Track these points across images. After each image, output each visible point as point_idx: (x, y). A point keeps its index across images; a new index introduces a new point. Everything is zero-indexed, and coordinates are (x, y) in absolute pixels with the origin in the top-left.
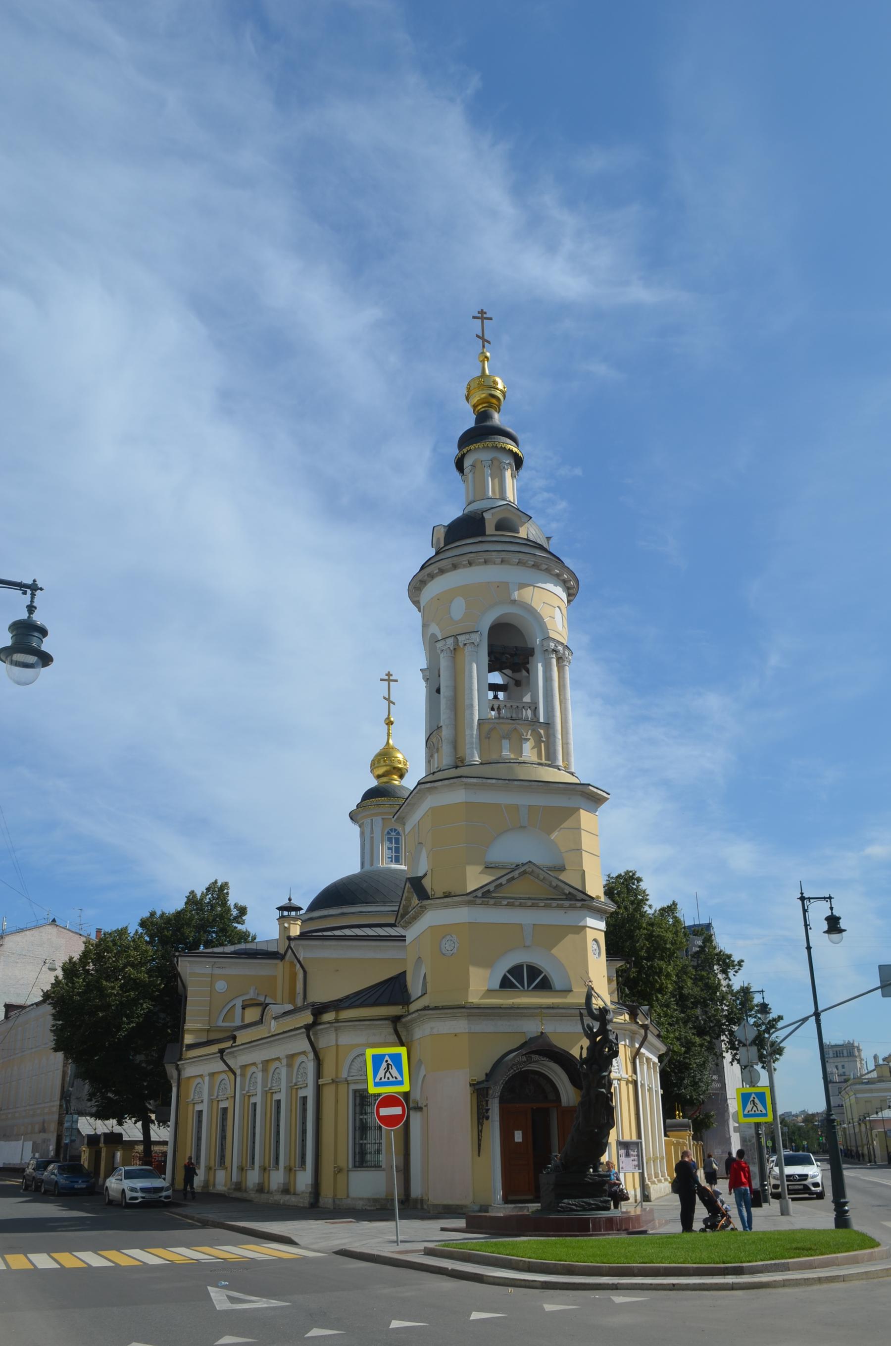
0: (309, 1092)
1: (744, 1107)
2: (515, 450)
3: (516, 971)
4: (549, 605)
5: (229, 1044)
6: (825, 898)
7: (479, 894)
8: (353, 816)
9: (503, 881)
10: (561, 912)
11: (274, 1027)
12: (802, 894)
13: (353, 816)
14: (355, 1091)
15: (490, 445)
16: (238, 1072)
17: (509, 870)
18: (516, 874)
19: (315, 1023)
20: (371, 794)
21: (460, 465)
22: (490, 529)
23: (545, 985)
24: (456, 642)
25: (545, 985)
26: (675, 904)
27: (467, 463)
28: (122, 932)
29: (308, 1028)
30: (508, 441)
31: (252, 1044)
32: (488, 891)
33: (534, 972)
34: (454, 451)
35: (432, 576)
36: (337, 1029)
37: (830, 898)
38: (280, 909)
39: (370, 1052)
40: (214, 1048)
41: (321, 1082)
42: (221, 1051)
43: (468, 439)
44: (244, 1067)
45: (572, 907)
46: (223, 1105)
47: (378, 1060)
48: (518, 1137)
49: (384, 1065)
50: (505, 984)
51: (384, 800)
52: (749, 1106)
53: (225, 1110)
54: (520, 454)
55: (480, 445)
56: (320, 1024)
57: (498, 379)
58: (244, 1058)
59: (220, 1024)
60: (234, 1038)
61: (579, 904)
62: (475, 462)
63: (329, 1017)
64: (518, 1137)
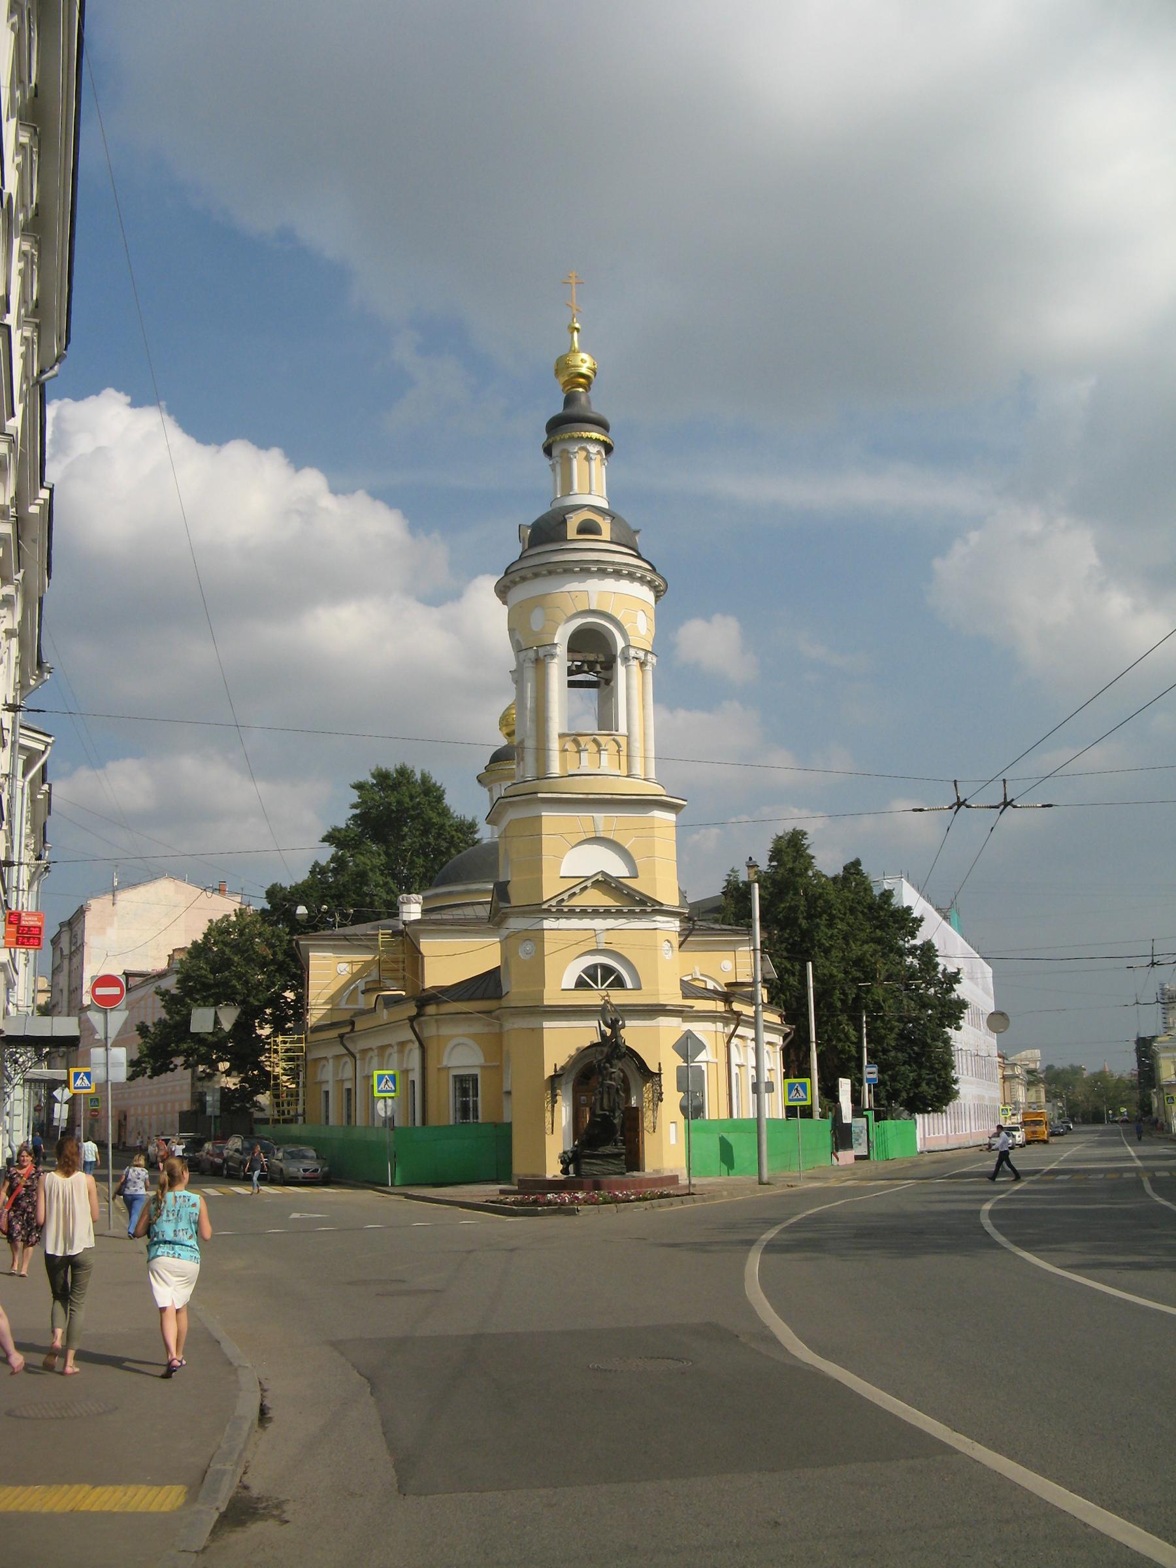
0: (416, 1076)
1: (790, 1093)
2: (602, 438)
3: (591, 971)
5: (348, 1029)
7: (554, 903)
9: (577, 890)
11: (554, 903)
13: (480, 780)
14: (455, 1077)
16: (358, 1056)
18: (589, 883)
19: (419, 1015)
21: (548, 451)
22: (572, 533)
23: (619, 983)
24: (537, 651)
25: (619, 983)
27: (556, 451)
28: (227, 917)
29: (412, 1019)
31: (368, 1032)
32: (563, 900)
33: (608, 971)
35: (515, 583)
36: (437, 1021)
38: (14, 1248)
39: (376, 1073)
40: (334, 1033)
42: (341, 1036)
43: (555, 425)
44: (364, 1051)
46: (348, 1085)
47: (381, 1078)
50: (581, 984)
52: (794, 1092)
53: (349, 1090)
54: (608, 441)
56: (423, 1015)
58: (362, 1044)
59: (343, 1005)
60: (353, 1023)
63: (431, 1009)
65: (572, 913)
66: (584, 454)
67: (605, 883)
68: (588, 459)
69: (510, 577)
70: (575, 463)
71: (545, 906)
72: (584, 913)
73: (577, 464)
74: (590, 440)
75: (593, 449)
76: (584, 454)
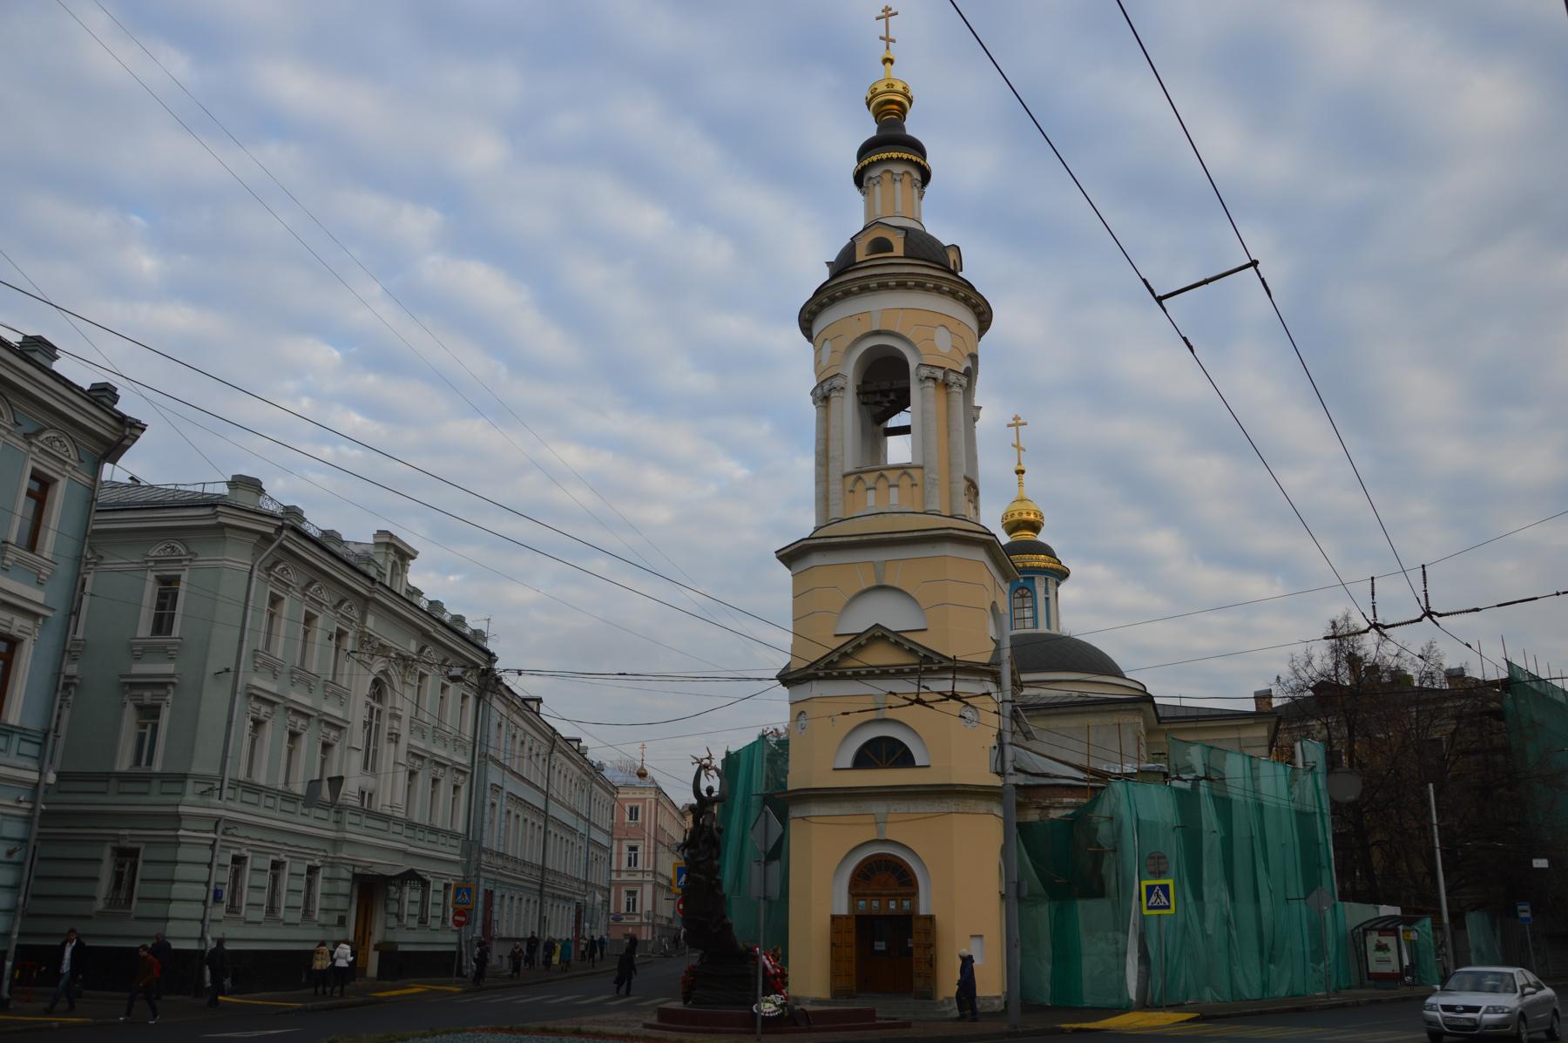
9: (849, 649)
21: (859, 179)
52: (1153, 898)
65: (842, 676)
67: (878, 635)
69: (829, 293)
71: (811, 671)
72: (856, 676)
75: (917, 175)
76: (887, 177)
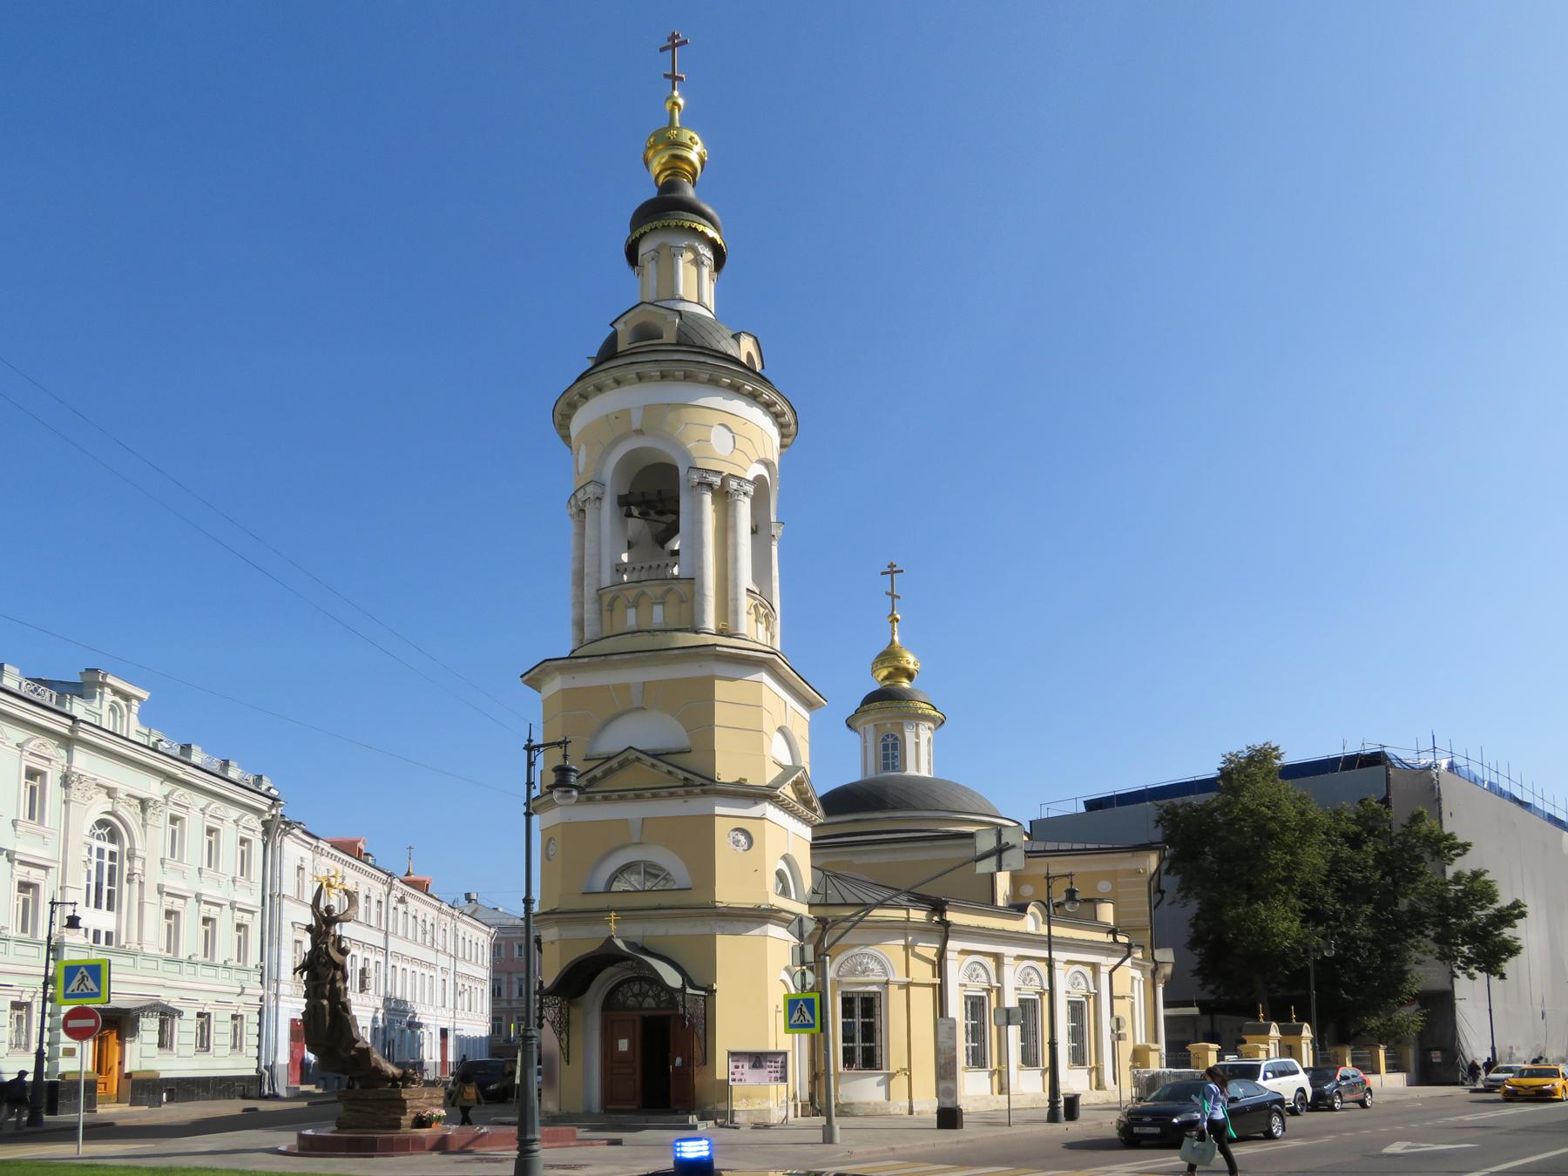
4: (735, 438)
6: (558, 744)
8: (850, 724)
10: (680, 801)
12: (530, 741)
13: (850, 724)
15: (673, 223)
17: (666, 758)
20: (871, 699)
26: (1470, 845)
27: (645, 248)
30: (695, 217)
34: (624, 234)
35: (585, 397)
37: (565, 743)
41: (12, 944)
45: (688, 794)
48: (623, 1045)
49: (79, 976)
51: (887, 703)
54: (719, 241)
55: (658, 224)
57: (687, 135)
61: (697, 790)
62: (661, 246)
64: (623, 1045)
66: (689, 256)
68: (698, 262)
70: (681, 262)
73: (684, 265)
74: (702, 236)
75: (707, 253)
76: (689, 256)
